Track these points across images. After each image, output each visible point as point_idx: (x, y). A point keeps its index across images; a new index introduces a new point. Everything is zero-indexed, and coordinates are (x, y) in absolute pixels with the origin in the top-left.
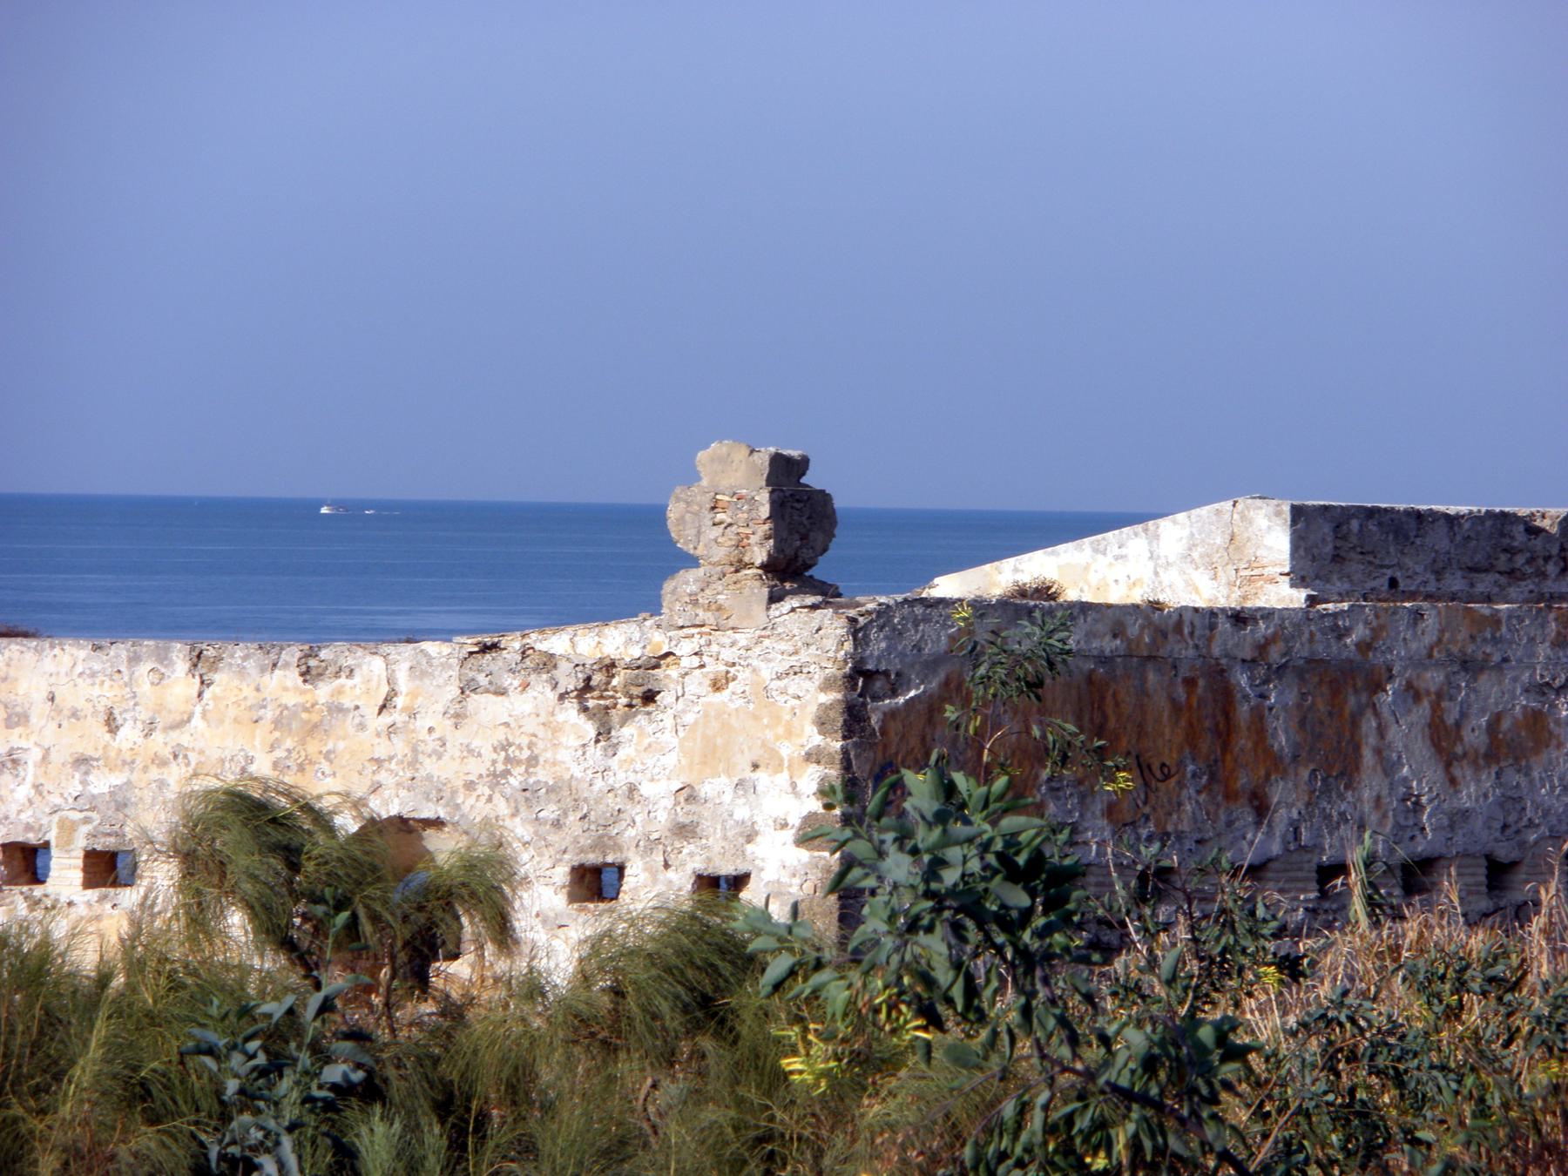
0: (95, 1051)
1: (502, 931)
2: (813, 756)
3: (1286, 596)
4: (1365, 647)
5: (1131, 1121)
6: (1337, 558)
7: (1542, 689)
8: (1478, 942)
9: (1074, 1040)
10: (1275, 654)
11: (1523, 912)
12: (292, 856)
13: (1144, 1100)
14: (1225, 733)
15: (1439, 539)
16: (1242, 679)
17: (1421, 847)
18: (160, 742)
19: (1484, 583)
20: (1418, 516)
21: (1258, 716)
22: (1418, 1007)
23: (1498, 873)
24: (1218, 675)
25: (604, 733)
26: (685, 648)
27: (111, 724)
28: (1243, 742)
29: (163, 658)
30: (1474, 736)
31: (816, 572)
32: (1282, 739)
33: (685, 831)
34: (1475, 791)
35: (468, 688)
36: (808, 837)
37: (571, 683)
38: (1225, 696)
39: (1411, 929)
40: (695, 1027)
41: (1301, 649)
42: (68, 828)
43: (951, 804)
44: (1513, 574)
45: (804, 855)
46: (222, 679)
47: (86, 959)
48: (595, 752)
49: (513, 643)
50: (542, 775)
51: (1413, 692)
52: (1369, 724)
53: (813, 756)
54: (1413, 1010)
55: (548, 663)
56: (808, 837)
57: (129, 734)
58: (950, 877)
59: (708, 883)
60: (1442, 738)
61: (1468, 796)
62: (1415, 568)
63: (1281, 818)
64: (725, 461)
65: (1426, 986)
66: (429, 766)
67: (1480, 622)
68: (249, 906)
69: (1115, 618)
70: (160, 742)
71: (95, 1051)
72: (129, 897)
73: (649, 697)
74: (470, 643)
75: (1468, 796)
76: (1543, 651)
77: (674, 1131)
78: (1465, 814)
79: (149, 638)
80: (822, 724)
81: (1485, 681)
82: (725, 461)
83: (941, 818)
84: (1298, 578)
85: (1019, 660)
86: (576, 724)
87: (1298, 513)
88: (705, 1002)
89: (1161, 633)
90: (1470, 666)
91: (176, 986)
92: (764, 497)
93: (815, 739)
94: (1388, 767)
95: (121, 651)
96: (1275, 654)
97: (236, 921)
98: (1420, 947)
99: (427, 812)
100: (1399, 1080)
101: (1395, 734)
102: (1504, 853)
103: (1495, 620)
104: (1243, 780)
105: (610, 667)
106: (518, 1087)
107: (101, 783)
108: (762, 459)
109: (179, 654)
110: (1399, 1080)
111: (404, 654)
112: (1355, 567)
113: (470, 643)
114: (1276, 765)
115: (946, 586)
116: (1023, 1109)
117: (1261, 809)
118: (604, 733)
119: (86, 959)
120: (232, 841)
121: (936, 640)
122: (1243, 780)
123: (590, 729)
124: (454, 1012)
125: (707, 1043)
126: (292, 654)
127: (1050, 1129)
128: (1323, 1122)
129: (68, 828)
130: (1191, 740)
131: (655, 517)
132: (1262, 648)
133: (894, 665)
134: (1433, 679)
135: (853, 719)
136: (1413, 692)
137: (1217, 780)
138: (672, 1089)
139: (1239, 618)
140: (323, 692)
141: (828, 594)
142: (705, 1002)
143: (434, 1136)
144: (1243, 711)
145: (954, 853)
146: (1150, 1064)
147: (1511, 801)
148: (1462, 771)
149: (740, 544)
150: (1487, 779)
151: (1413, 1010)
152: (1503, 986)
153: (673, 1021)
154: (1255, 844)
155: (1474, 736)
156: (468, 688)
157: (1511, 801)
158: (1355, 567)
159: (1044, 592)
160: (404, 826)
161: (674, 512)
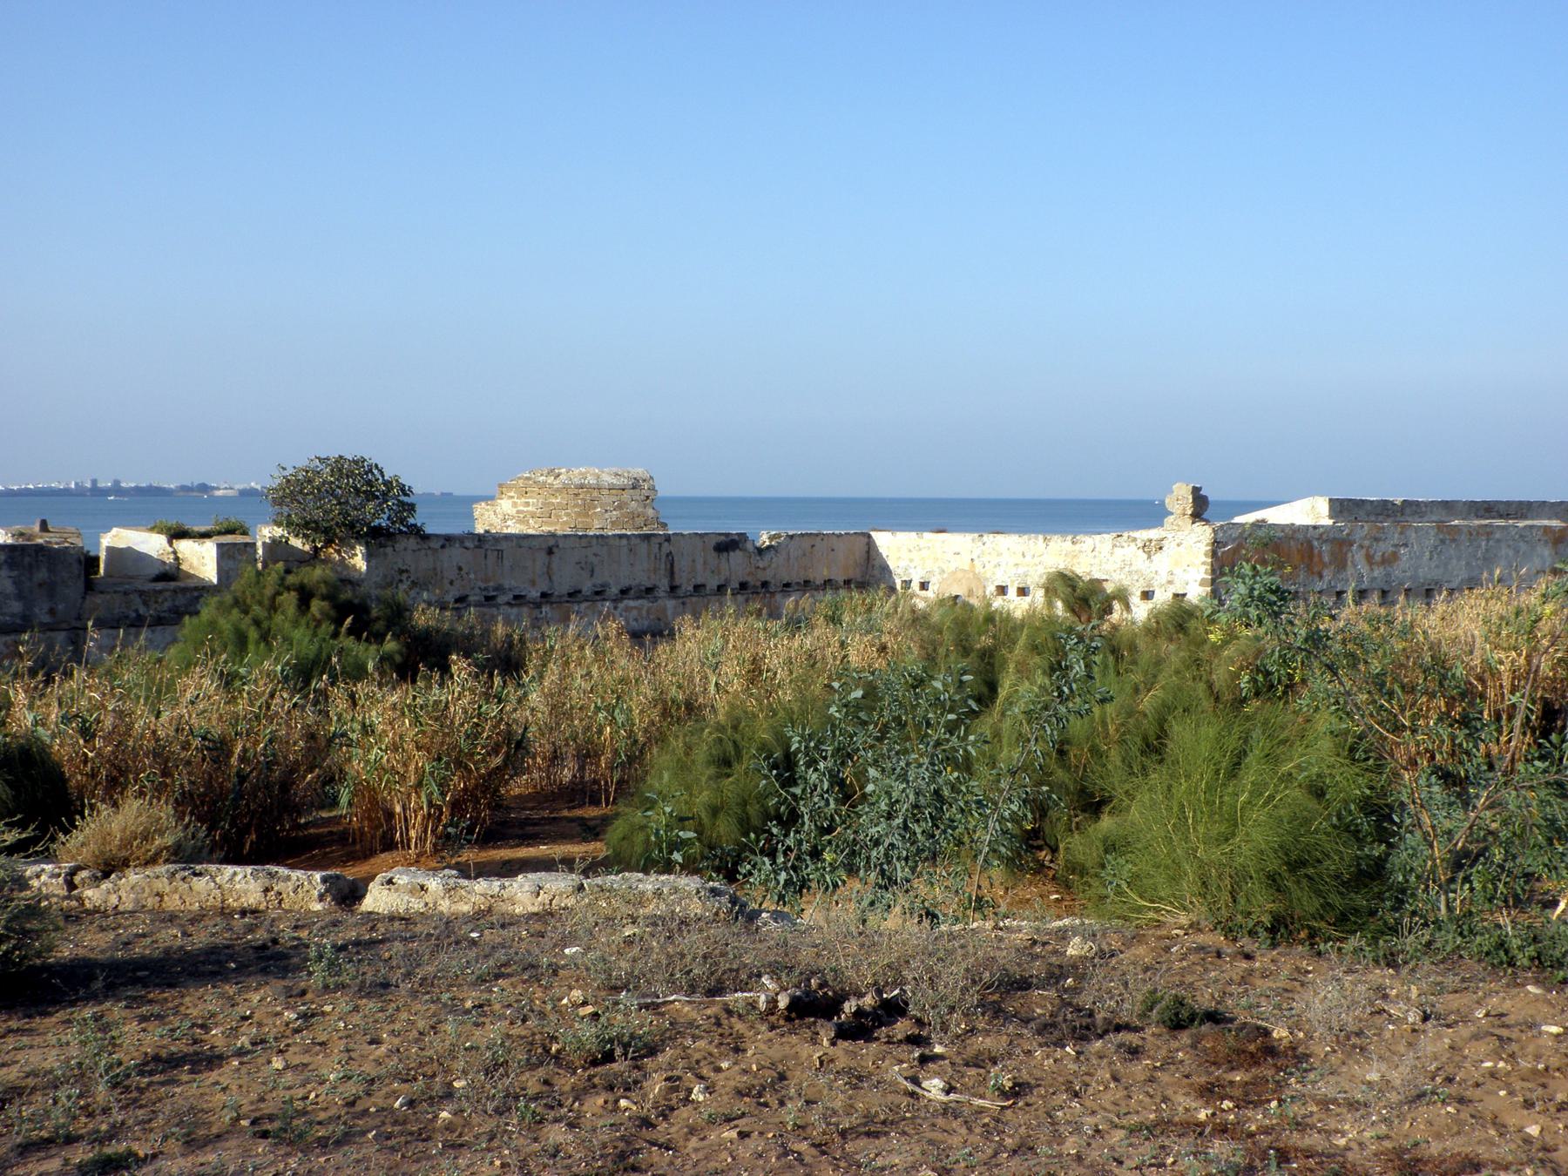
0: (1024, 637)
1: (1127, 607)
2: (1204, 563)
3: (1330, 522)
4: (1348, 535)
5: (1111, 623)
6: (1341, 512)
7: (1396, 546)
8: (1382, 611)
9: (1287, 635)
10: (1324, 537)
11: (1394, 603)
12: (1074, 588)
13: (1305, 650)
14: (1311, 557)
15: (1369, 507)
16: (1316, 543)
17: (1363, 587)
18: (1037, 560)
19: (1380, 518)
20: (1363, 501)
21: (1320, 553)
22: (1366, 627)
23: (1384, 593)
24: (1309, 543)
25: (1149, 557)
26: (1169, 536)
27: (1024, 555)
28: (1316, 559)
29: (1036, 539)
30: (1378, 558)
31: (1204, 516)
32: (1326, 559)
33: (1170, 582)
34: (1378, 572)
35: (1114, 546)
36: (1202, 584)
37: (1141, 545)
38: (1311, 547)
39: (1364, 608)
40: (1178, 632)
41: (1331, 536)
42: (1013, 582)
43: (1256, 573)
44: (1388, 516)
45: (1201, 589)
46: (1052, 544)
47: (1018, 614)
48: (1147, 562)
49: (1126, 535)
50: (1134, 568)
51: (1361, 547)
52: (1350, 555)
53: (1204, 563)
54: (1364, 627)
55: (1135, 540)
56: (1202, 584)
57: (1028, 557)
58: (1256, 593)
59: (1176, 596)
60: (1369, 559)
61: (1376, 573)
62: (1362, 513)
63: (1326, 579)
64: (1180, 488)
65: (1370, 621)
66: (1104, 566)
67: (1380, 528)
68: (1063, 601)
69: (1282, 528)
70: (1037, 560)
71: (1024, 637)
72: (1028, 599)
73: (1161, 548)
74: (1115, 535)
75: (1376, 573)
76: (1396, 535)
77: (1173, 658)
78: (1375, 578)
79: (545, 844)
80: (1206, 555)
81: (1381, 543)
82: (1180, 488)
83: (1254, 576)
84: (1331, 517)
85: (1262, 538)
86: (1143, 556)
87: (1330, 500)
88: (1180, 625)
89: (1294, 531)
90: (1377, 540)
91: (1044, 621)
92: (1190, 497)
93: (1204, 559)
94: (1355, 566)
95: (1026, 537)
96: (1324, 537)
97: (1059, 604)
98: (1366, 612)
99: (1104, 577)
100: (1362, 646)
101: (1357, 557)
102: (1386, 588)
103: (1383, 528)
104: (1316, 569)
105: (1150, 541)
106: (1133, 648)
107: (1021, 570)
108: (1190, 487)
109: (1041, 537)
110: (1362, 646)
111: (1098, 537)
112: (1346, 514)
113: (1115, 535)
114: (1325, 565)
115: (1238, 520)
116: (1273, 651)
117: (1321, 577)
118: (1149, 557)
119: (1018, 614)
120: (1059, 585)
121: (1235, 534)
122: (1316, 569)
123: (1145, 556)
124: (1115, 628)
125: (1181, 636)
126: (1070, 538)
127: (1280, 656)
128: (1341, 657)
129: (1013, 582)
130: (1303, 557)
131: (1162, 503)
132: (1321, 535)
133: (1224, 540)
134: (1367, 543)
135: (1214, 554)
136: (1361, 547)
137: (1309, 568)
138: (1172, 647)
139: (1315, 527)
140: (1077, 547)
141: (1207, 522)
142: (1180, 625)
143: (1111, 658)
144: (1316, 551)
145: (1257, 586)
146: (1306, 640)
147: (1388, 575)
148: (1375, 567)
149: (1184, 509)
150: (1382, 569)
151: (1364, 627)
152: (1389, 623)
153: (1172, 630)
154: (1319, 585)
155: (1378, 558)
156: (1114, 546)
157: (1388, 575)
158: (1346, 514)
159: (1263, 521)
160: (1099, 582)
161: (1167, 501)
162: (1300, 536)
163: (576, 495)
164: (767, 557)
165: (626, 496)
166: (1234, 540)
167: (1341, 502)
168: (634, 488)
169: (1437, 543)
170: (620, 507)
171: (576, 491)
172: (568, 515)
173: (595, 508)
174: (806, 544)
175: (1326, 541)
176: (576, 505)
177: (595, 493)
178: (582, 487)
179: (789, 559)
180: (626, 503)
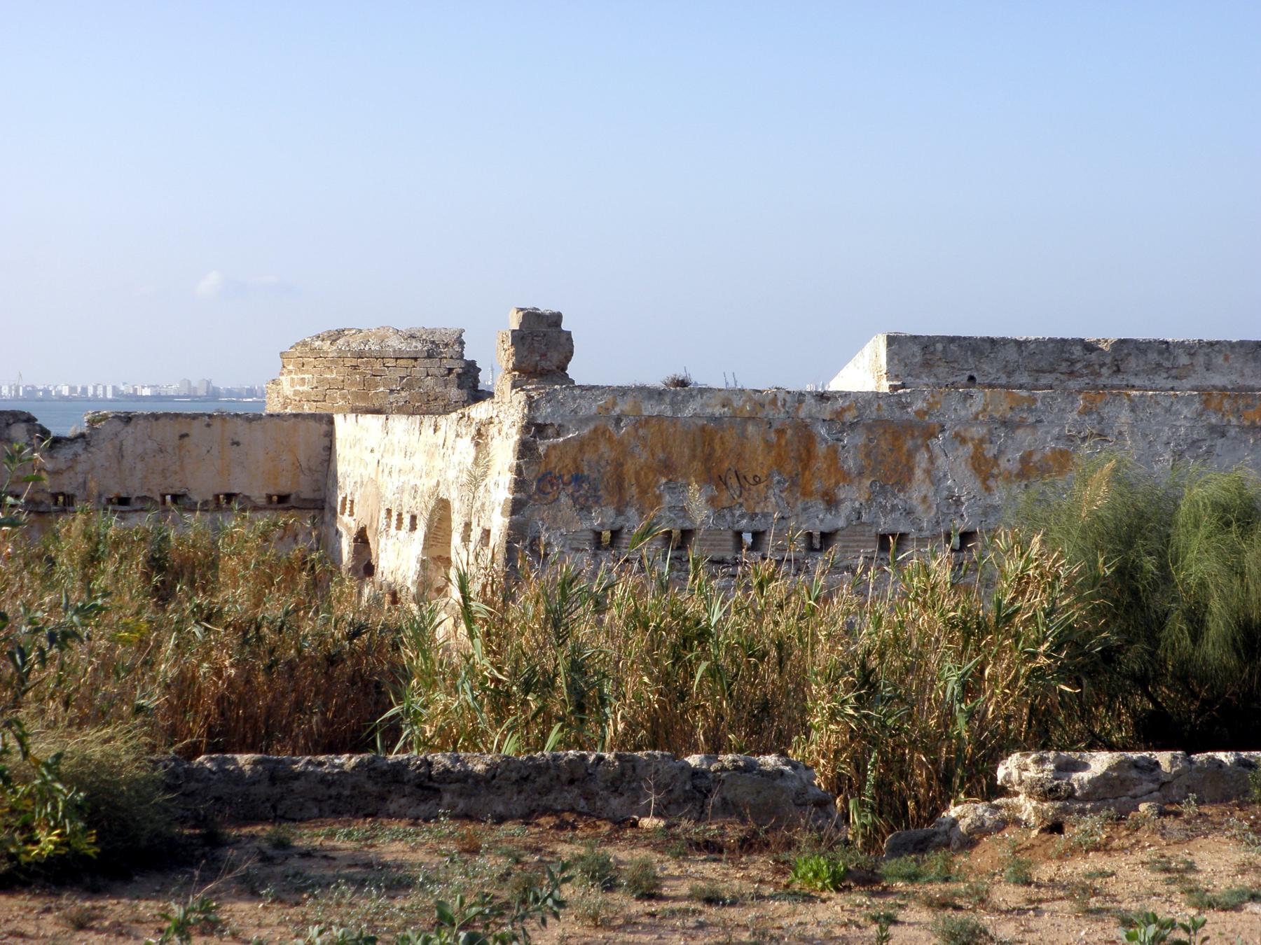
3: (885, 387)
15: (1012, 354)
28: (820, 464)
32: (850, 463)
52: (922, 458)
63: (846, 508)
81: (1020, 433)
96: (849, 417)
132: (840, 413)
134: (978, 432)
144: (821, 449)
162: (779, 415)
163: (355, 367)
164: (64, 454)
165: (419, 370)
166: (587, 420)
167: (927, 344)
168: (430, 356)
170: (409, 386)
171: (354, 362)
172: (344, 397)
173: (376, 387)
174: (169, 432)
175: (853, 426)
176: (353, 384)
177: (378, 365)
178: (360, 355)
179: (121, 455)
180: (419, 380)
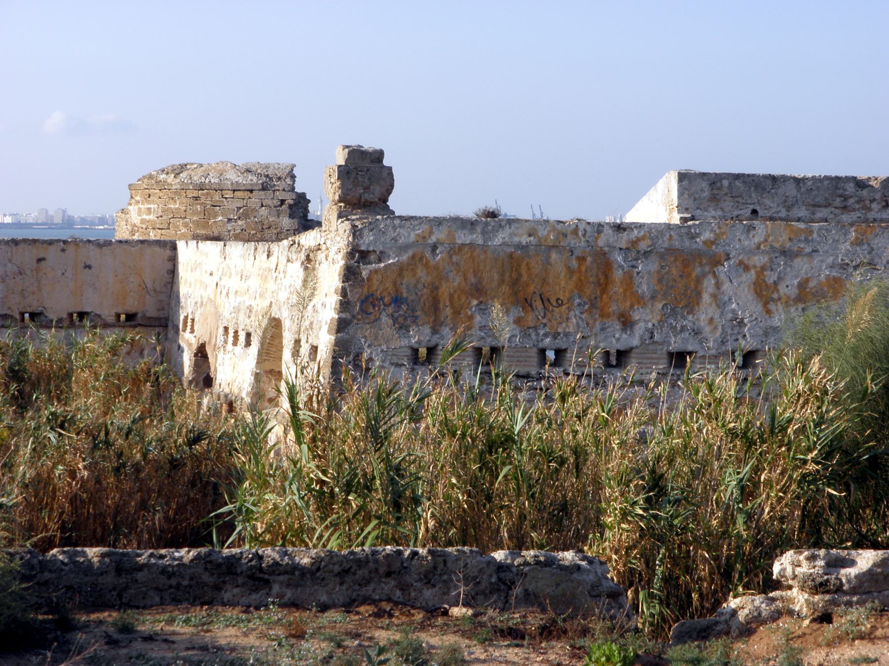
3: (676, 219)
14: (604, 282)
15: (791, 190)
20: (773, 179)
28: (617, 288)
30: (789, 288)
52: (709, 283)
96: (643, 246)
122: (613, 308)
130: (580, 286)
132: (635, 243)
144: (618, 275)
163: (196, 198)
167: (714, 180)
168: (264, 188)
169: (578, 253)
170: (245, 216)
172: (186, 225)
173: (215, 216)
174: (28, 256)
177: (217, 197)
180: (255, 210)
